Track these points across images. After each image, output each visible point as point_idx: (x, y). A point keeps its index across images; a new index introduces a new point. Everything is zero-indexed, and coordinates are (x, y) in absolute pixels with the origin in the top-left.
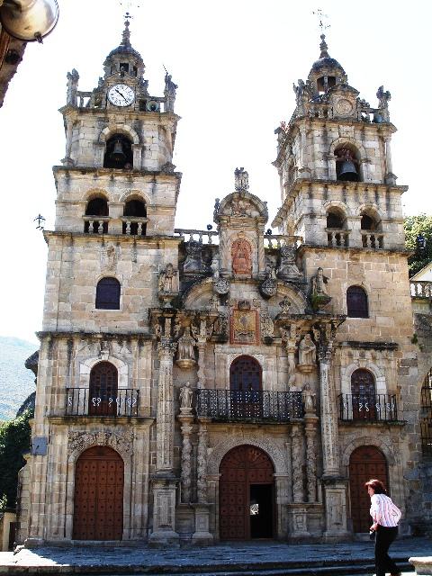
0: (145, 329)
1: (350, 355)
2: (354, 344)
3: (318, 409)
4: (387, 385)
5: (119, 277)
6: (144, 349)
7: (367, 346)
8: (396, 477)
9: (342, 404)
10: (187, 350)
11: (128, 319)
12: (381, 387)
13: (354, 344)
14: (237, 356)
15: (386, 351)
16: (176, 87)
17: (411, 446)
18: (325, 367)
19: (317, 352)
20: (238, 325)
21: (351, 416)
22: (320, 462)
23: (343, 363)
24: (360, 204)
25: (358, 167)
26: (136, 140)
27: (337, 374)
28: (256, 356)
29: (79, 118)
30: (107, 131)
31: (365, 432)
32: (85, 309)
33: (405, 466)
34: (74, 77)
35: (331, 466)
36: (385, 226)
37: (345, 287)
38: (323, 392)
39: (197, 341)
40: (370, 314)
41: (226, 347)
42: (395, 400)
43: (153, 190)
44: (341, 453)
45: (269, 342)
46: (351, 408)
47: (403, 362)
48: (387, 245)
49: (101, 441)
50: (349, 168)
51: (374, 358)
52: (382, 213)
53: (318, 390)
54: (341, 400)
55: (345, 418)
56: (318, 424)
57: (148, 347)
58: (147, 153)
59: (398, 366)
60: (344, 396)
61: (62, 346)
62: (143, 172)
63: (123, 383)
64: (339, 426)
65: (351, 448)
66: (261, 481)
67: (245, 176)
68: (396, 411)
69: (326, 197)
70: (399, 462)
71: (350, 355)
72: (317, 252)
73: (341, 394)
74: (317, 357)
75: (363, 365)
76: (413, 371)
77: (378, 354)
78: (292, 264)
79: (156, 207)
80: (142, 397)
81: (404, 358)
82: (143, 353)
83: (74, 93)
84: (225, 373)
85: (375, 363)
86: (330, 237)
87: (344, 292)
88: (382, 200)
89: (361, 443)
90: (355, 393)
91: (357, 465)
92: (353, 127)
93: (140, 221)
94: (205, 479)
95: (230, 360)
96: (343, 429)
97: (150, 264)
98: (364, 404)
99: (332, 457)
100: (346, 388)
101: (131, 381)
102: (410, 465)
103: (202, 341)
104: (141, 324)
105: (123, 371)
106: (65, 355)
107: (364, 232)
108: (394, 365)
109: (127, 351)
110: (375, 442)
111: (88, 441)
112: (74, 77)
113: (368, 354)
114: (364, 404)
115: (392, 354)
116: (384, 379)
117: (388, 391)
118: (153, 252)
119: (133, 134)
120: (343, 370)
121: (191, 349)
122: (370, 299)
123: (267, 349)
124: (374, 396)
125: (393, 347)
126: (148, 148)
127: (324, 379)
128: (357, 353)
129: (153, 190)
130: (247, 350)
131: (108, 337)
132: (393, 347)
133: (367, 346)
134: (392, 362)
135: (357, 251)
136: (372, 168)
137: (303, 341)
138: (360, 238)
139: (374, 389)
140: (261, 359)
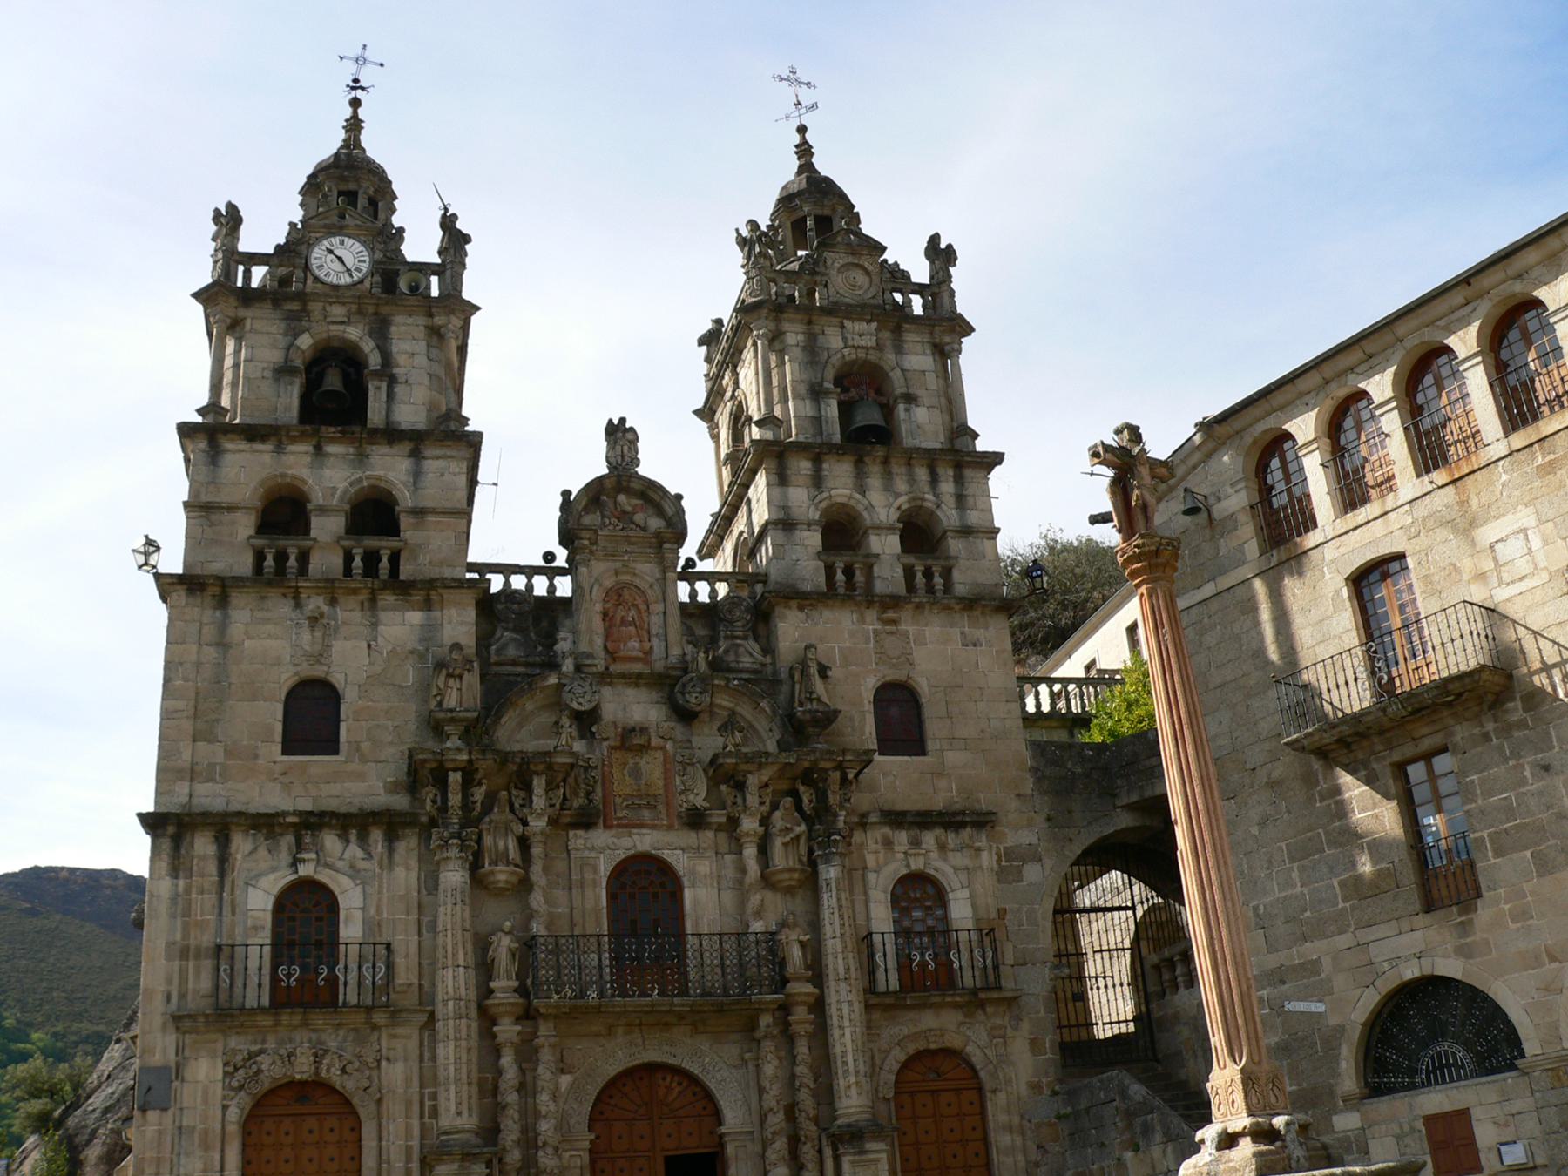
0: (401, 802)
1: (888, 844)
2: (896, 819)
3: (817, 972)
4: (974, 906)
5: (337, 679)
6: (401, 847)
7: (923, 820)
8: (1003, 1118)
9: (871, 956)
10: (501, 844)
11: (361, 776)
12: (961, 911)
13: (896, 819)
14: (622, 855)
15: (968, 830)
16: (466, 239)
17: (1035, 1045)
18: (830, 873)
19: (810, 839)
20: (622, 785)
21: (894, 984)
22: (826, 1094)
23: (871, 860)
24: (898, 495)
25: (888, 410)
26: (374, 361)
27: (858, 888)
28: (666, 855)
29: (242, 312)
30: (305, 341)
31: (928, 1020)
32: (256, 757)
33: (1024, 1090)
34: (229, 221)
35: (852, 1102)
36: (955, 545)
37: (870, 684)
38: (828, 930)
39: (525, 823)
40: (931, 745)
41: (600, 837)
42: (993, 942)
43: (417, 474)
44: (874, 1069)
45: (695, 820)
46: (892, 963)
47: (1009, 854)
48: (960, 589)
49: (302, 1069)
50: (868, 416)
51: (942, 847)
52: (948, 516)
53: (815, 926)
54: (870, 946)
55: (881, 987)
56: (819, 1006)
57: (407, 846)
58: (399, 390)
59: (999, 861)
60: (877, 939)
61: (203, 845)
62: (392, 434)
63: (351, 930)
64: (868, 1008)
65: (898, 1056)
66: (692, 1143)
67: (629, 436)
68: (996, 967)
69: (817, 481)
70: (1008, 1082)
71: (888, 844)
72: (801, 608)
73: (870, 934)
74: (810, 852)
75: (917, 864)
76: (1032, 873)
77: (951, 839)
78: (745, 638)
79: (420, 513)
80: (399, 961)
81: (1009, 844)
82: (397, 857)
83: (230, 257)
84: (598, 898)
85: (945, 860)
86: (830, 571)
87: (868, 696)
88: (947, 487)
89: (921, 1045)
90: (903, 933)
91: (912, 1093)
92: (874, 325)
93: (385, 545)
94: (556, 1149)
95: (605, 867)
96: (876, 1015)
97: (409, 646)
98: (922, 954)
99: (852, 1079)
100: (881, 918)
101: (371, 925)
102: (1035, 1087)
103: (538, 824)
104: (393, 788)
105: (350, 897)
106: (212, 868)
107: (910, 559)
108: (987, 859)
109: (360, 853)
110: (954, 1042)
111: (272, 1069)
112: (229, 221)
113: (929, 839)
114: (922, 954)
115: (982, 840)
116: (965, 893)
117: (977, 920)
118: (416, 617)
119: (368, 346)
120: (872, 877)
121: (512, 844)
122: (928, 712)
123: (690, 837)
124: (946, 932)
125: (983, 821)
126: (401, 379)
127: (829, 900)
128: (902, 838)
129: (417, 474)
130: (644, 842)
131: (311, 823)
132: (983, 821)
133: (923, 820)
134: (985, 855)
135: (891, 603)
136: (921, 414)
137: (777, 814)
138: (899, 571)
139: (945, 918)
140: (680, 861)
